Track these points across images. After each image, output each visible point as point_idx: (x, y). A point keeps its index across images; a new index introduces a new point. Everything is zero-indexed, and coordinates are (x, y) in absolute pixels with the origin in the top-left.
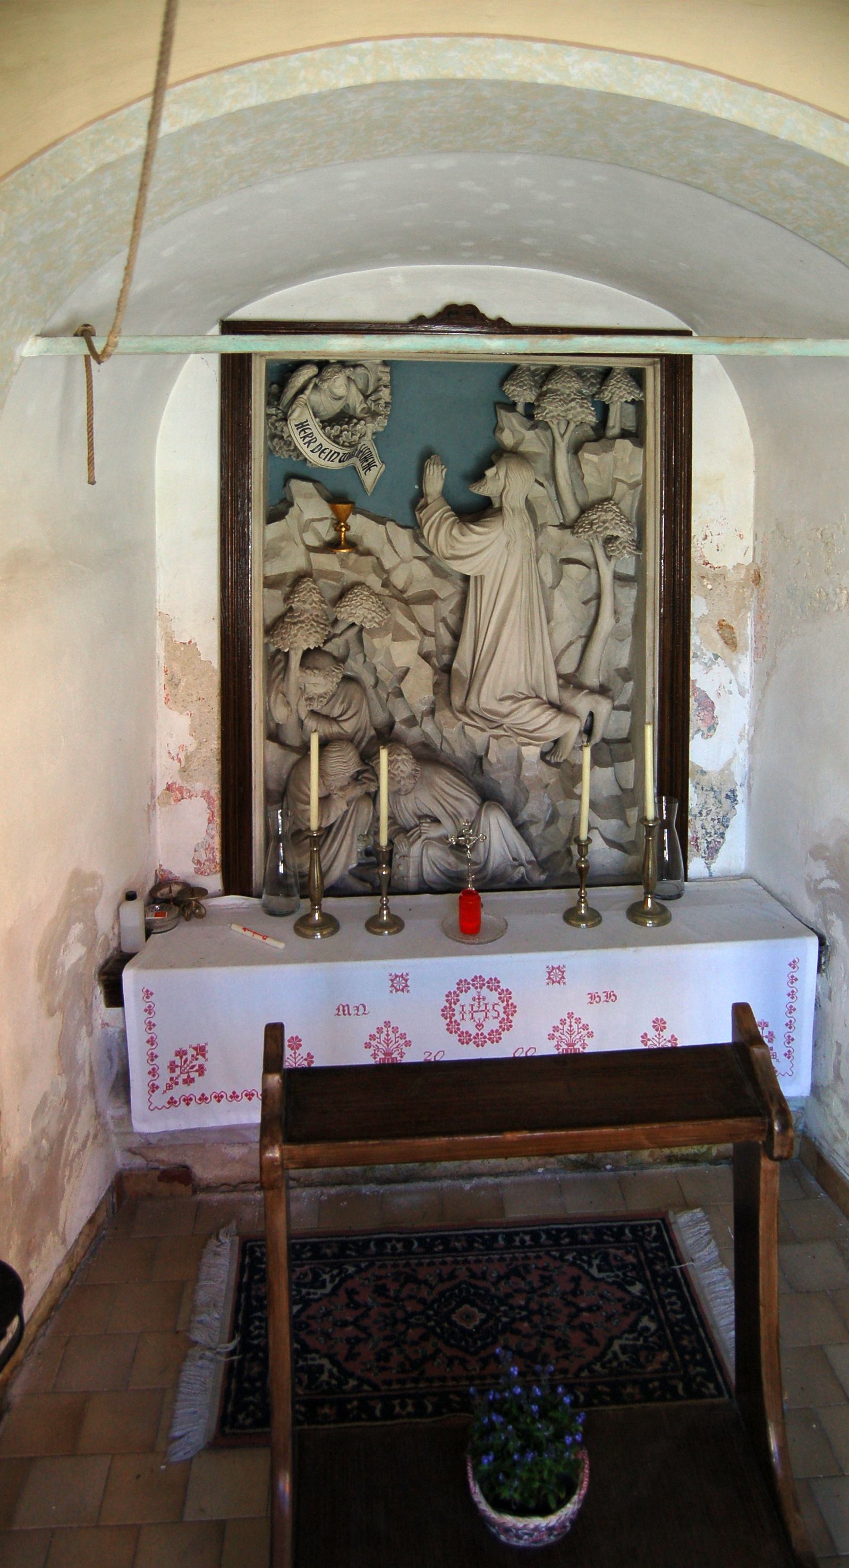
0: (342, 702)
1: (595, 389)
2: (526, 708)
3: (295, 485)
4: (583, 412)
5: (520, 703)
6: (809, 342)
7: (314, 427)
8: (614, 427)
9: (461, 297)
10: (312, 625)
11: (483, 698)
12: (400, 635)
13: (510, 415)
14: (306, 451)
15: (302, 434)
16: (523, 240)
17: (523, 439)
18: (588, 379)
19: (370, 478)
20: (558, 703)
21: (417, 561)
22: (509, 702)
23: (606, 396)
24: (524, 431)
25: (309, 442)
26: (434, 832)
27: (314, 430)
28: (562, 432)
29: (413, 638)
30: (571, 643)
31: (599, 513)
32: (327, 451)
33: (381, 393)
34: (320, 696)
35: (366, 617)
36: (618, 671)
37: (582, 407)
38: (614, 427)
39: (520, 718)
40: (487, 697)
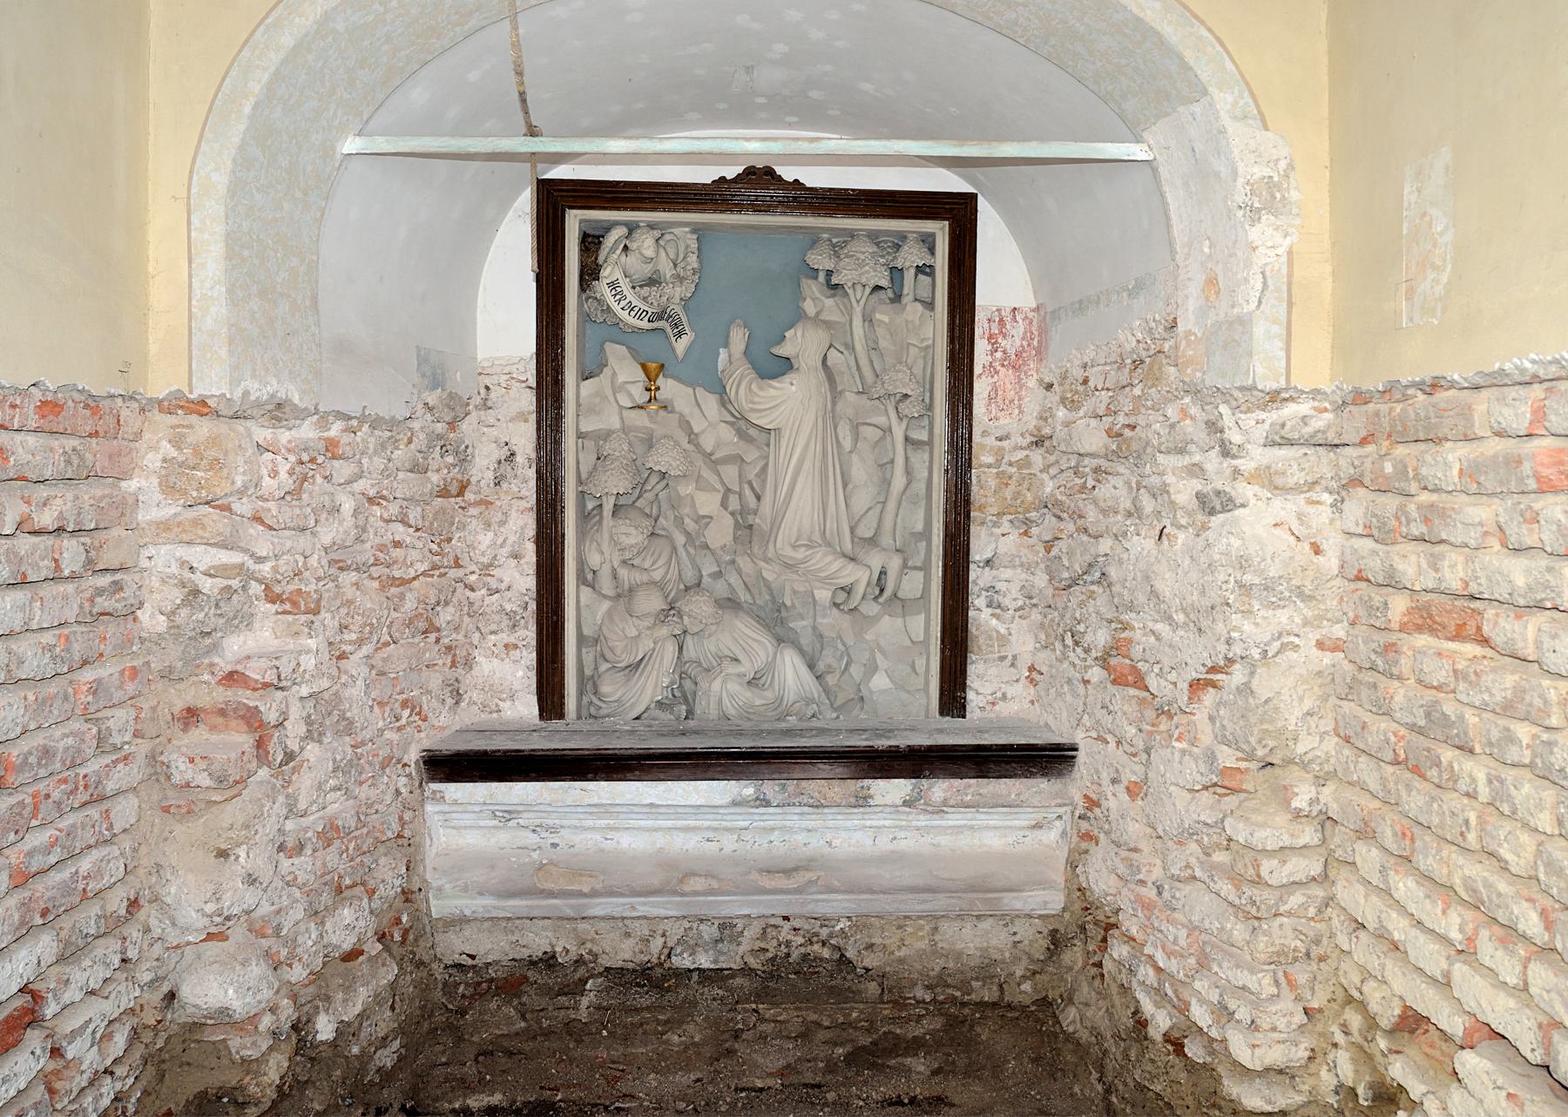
2: (819, 555)
3: (608, 346)
6: (1034, 144)
7: (625, 286)
11: (779, 544)
12: (701, 484)
16: (811, 94)
19: (681, 345)
26: (732, 669)
36: (913, 534)
40: (783, 544)
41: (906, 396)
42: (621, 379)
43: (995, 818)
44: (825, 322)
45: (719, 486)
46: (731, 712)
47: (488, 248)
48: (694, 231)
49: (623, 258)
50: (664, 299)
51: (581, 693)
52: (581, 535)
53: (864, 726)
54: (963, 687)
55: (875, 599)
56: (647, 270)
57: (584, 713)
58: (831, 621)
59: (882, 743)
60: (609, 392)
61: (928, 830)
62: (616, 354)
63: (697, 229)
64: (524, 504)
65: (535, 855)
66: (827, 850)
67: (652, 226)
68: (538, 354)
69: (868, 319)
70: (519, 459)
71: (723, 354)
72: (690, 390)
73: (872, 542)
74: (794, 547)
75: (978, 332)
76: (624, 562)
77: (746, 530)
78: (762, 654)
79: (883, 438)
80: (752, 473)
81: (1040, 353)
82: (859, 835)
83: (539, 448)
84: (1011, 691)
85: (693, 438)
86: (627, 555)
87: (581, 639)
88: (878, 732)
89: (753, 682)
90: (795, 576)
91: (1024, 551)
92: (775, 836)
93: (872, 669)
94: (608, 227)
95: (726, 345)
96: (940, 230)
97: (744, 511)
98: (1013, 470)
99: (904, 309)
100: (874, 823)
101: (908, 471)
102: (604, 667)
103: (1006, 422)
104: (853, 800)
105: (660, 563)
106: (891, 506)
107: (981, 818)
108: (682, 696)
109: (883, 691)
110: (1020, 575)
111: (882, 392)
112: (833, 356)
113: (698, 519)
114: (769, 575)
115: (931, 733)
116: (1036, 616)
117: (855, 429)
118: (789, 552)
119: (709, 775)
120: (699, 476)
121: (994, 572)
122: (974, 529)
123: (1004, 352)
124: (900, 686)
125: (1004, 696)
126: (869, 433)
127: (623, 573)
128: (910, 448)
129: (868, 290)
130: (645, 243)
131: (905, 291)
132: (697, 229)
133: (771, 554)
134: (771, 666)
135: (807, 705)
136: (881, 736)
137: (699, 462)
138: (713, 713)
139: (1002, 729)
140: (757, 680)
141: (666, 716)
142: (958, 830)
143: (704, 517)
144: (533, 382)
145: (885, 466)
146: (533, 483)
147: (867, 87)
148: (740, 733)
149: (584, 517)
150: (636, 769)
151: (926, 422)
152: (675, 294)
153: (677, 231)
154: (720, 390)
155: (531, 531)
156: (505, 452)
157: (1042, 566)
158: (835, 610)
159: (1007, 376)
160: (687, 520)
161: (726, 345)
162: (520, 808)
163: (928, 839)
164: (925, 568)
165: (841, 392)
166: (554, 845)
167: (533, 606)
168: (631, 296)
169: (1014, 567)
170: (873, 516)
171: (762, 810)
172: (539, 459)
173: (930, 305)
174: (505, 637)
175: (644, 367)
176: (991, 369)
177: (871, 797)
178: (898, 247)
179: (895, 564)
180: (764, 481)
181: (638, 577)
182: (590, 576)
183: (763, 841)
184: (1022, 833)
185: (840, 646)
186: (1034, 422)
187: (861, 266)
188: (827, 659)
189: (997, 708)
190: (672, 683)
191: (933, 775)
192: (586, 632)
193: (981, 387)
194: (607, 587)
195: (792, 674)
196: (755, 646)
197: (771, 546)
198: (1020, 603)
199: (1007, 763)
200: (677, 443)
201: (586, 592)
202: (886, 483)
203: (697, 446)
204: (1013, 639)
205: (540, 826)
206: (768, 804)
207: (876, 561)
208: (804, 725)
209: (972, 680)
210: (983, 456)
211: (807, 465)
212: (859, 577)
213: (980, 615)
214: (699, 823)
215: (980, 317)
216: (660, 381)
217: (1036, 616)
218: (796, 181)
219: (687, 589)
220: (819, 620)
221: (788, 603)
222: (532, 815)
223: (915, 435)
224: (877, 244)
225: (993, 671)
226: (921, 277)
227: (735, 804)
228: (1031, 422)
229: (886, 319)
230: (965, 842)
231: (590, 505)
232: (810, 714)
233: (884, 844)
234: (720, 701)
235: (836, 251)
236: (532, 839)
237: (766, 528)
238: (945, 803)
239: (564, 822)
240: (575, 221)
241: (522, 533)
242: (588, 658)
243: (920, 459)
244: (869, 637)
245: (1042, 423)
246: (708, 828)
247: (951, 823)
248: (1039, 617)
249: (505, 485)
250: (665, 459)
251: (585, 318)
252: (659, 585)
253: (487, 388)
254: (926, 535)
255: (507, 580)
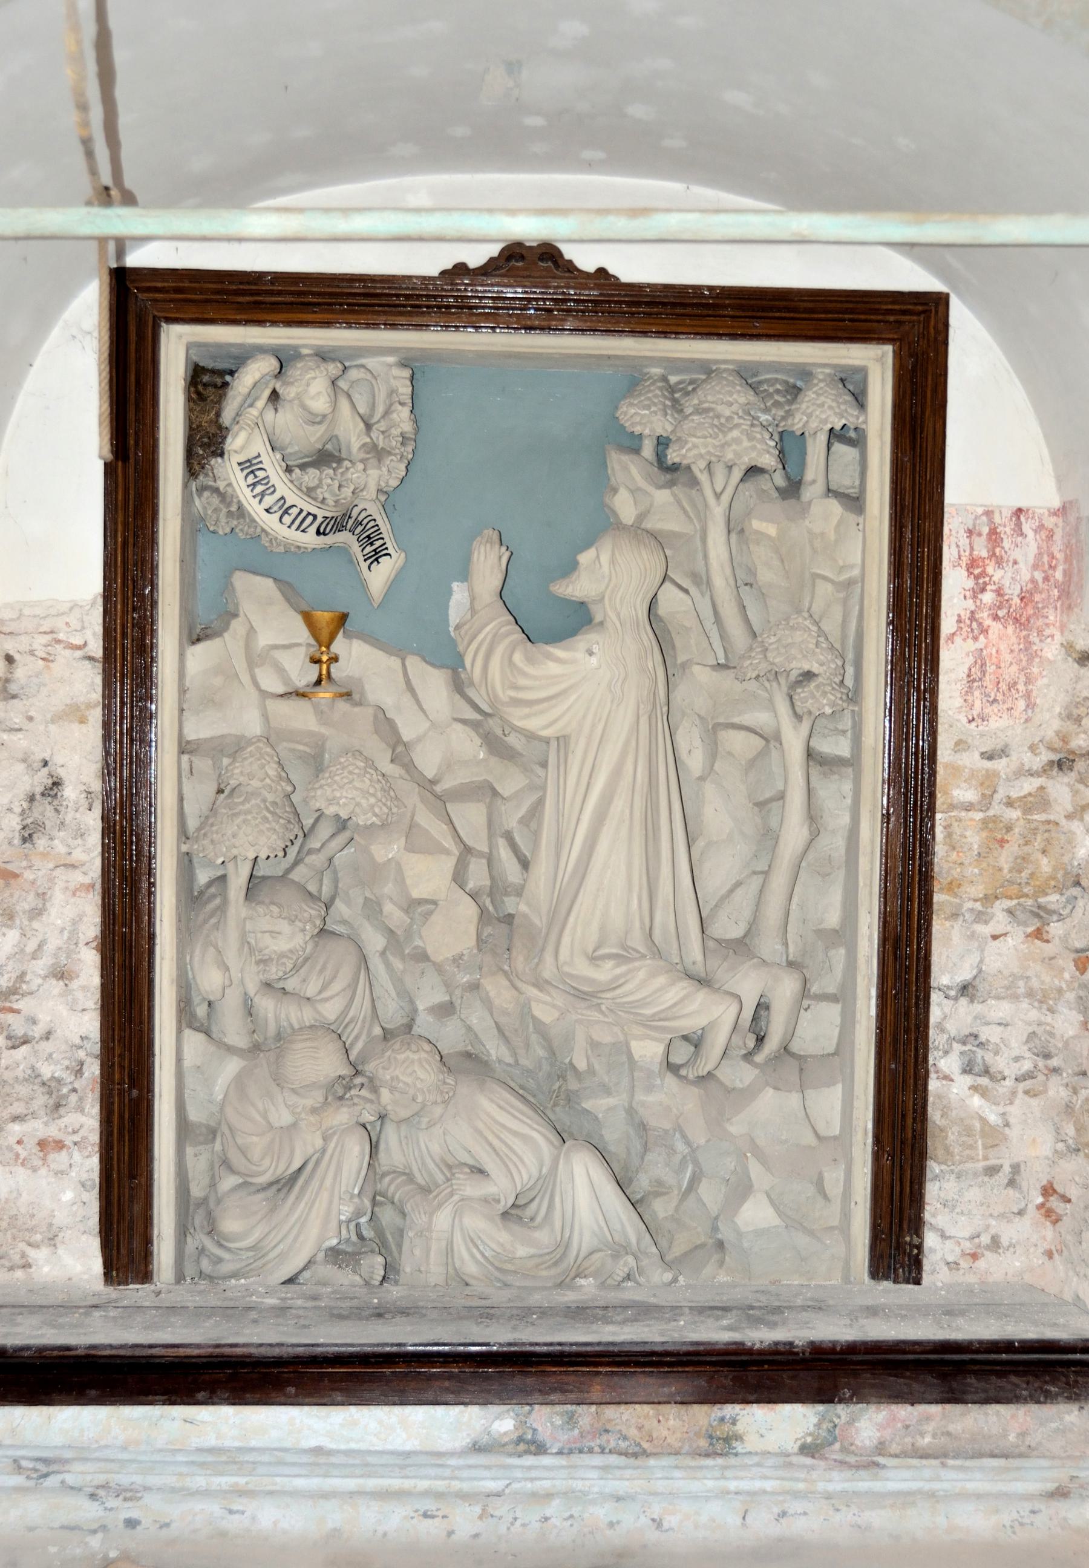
0: (321, 971)
1: (781, 413)
2: (642, 974)
3: (242, 581)
4: (754, 448)
5: (631, 966)
8: (814, 482)
9: (529, 229)
10: (265, 819)
12: (416, 841)
13: (625, 458)
14: (255, 508)
15: (251, 479)
17: (651, 505)
18: (771, 395)
20: (703, 975)
21: (459, 727)
22: (610, 964)
23: (797, 424)
24: (651, 489)
25: (263, 494)
26: (471, 1188)
27: (271, 472)
28: (718, 490)
29: (447, 852)
30: (738, 884)
31: (780, 633)
32: (294, 511)
33: (395, 415)
34: (282, 955)
35: (358, 804)
36: (820, 933)
37: (751, 438)
38: (814, 482)
39: (632, 993)
40: (571, 953)
41: (809, 675)
42: (264, 639)
43: (977, 1478)
44: (654, 535)
45: (448, 843)
46: (471, 1268)
47: (13, 398)
48: (403, 365)
49: (270, 415)
50: (347, 492)
51: (183, 1231)
52: (186, 932)
53: (725, 1299)
54: (917, 1225)
55: (748, 1056)
56: (314, 437)
57: (190, 1270)
58: (667, 1099)
59: (760, 1336)
60: (240, 665)
61: (847, 1498)
62: (255, 593)
63: (410, 362)
64: (79, 878)
65: (95, 1542)
66: (653, 1536)
67: (323, 356)
68: (108, 595)
69: (734, 528)
70: (70, 793)
71: (459, 594)
72: (395, 662)
73: (741, 948)
74: (594, 959)
75: (949, 554)
76: (268, 985)
77: (501, 925)
78: (530, 1159)
79: (764, 753)
80: (512, 818)
81: (1068, 595)
82: (714, 1508)
83: (107, 771)
84: (1009, 1232)
85: (400, 751)
86: (274, 972)
87: (184, 1129)
88: (751, 1313)
89: (513, 1214)
90: (595, 1015)
91: (1035, 968)
92: (553, 1509)
93: (741, 1190)
94: (243, 356)
95: (465, 575)
96: (876, 363)
97: (497, 889)
98: (1014, 814)
99: (805, 509)
100: (745, 1485)
101: (813, 816)
102: (229, 1182)
103: (1002, 725)
104: (703, 1443)
105: (336, 987)
106: (779, 881)
107: (950, 1478)
108: (373, 1239)
109: (760, 1233)
110: (1031, 1012)
111: (764, 667)
112: (671, 601)
113: (411, 905)
114: (544, 1013)
115: (853, 1316)
116: (1056, 1090)
117: (713, 731)
118: (582, 968)
119: (430, 1396)
120: (412, 825)
121: (977, 1007)
122: (939, 926)
123: (999, 592)
124: (793, 1220)
125: (995, 1244)
126: (738, 743)
127: (266, 1005)
128: (815, 771)
129: (737, 474)
130: (312, 388)
131: (809, 475)
132: (410, 362)
133: (548, 971)
134: (546, 1183)
135: (616, 1256)
136: (756, 1322)
137: (412, 796)
138: (435, 1273)
139: (991, 1308)
140: (517, 1219)
141: (345, 1278)
142: (905, 1499)
143: (421, 902)
144: (96, 648)
145: (766, 805)
146: (95, 839)
147: (736, 97)
148: (486, 1314)
149: (192, 899)
150: (289, 1382)
151: (847, 723)
152: (365, 483)
153: (371, 362)
154: (451, 662)
155: (91, 925)
156: (41, 779)
157: (1071, 996)
158: (670, 1079)
159: (1002, 638)
160: (388, 908)
161: (465, 575)
162: (68, 1454)
163: (846, 1517)
164: (843, 997)
165: (684, 666)
166: (131, 1524)
167: (93, 1069)
168: (283, 488)
169: (1015, 998)
170: (744, 899)
171: (529, 1460)
172: (107, 794)
173: (855, 502)
174: (38, 1128)
175: (308, 618)
176: (973, 625)
177: (738, 1437)
178: (794, 392)
179: (786, 989)
180: (536, 835)
181: (295, 1015)
182: (201, 1011)
183: (531, 1516)
184: (1028, 1506)
185: (680, 1147)
186: (1056, 724)
187: (722, 429)
188: (657, 1168)
189: (981, 1264)
190: (358, 1214)
191: (859, 1396)
192: (194, 1115)
193: (954, 659)
194: (233, 1028)
195: (586, 1196)
196: (517, 1144)
197: (548, 958)
198: (1027, 1066)
199: (1001, 1375)
200: (370, 763)
201: (194, 1041)
202: (769, 838)
203: (410, 767)
204: (1013, 1133)
205: (105, 1486)
206: (538, 1448)
207: (749, 985)
208: (612, 1297)
209: (933, 1212)
210: (955, 789)
211: (619, 804)
212: (716, 1015)
213: (949, 1086)
214: (407, 1484)
215: (953, 527)
216: (339, 645)
217: (1056, 1090)
218: (602, 272)
219: (388, 1035)
220: (640, 1096)
221: (581, 1065)
222: (89, 1467)
223: (827, 746)
224: (754, 388)
225: (974, 1194)
226: (839, 448)
227: (477, 1448)
228: (1050, 723)
229: (771, 530)
230: (920, 1522)
231: (203, 877)
232: (620, 1272)
233: (763, 1524)
234: (449, 1250)
235: (675, 398)
236: (89, 1512)
237: (539, 921)
238: (881, 1449)
239: (152, 1480)
240: (177, 345)
241: (74, 933)
242: (198, 1162)
243: (834, 794)
244: (736, 1127)
245: (1071, 727)
246: (426, 1493)
247: (892, 1486)
248: (1064, 1093)
249: (41, 842)
250: (346, 794)
251: (194, 527)
252: (335, 1032)
253: (9, 659)
254: (843, 935)
255: (44, 1018)
